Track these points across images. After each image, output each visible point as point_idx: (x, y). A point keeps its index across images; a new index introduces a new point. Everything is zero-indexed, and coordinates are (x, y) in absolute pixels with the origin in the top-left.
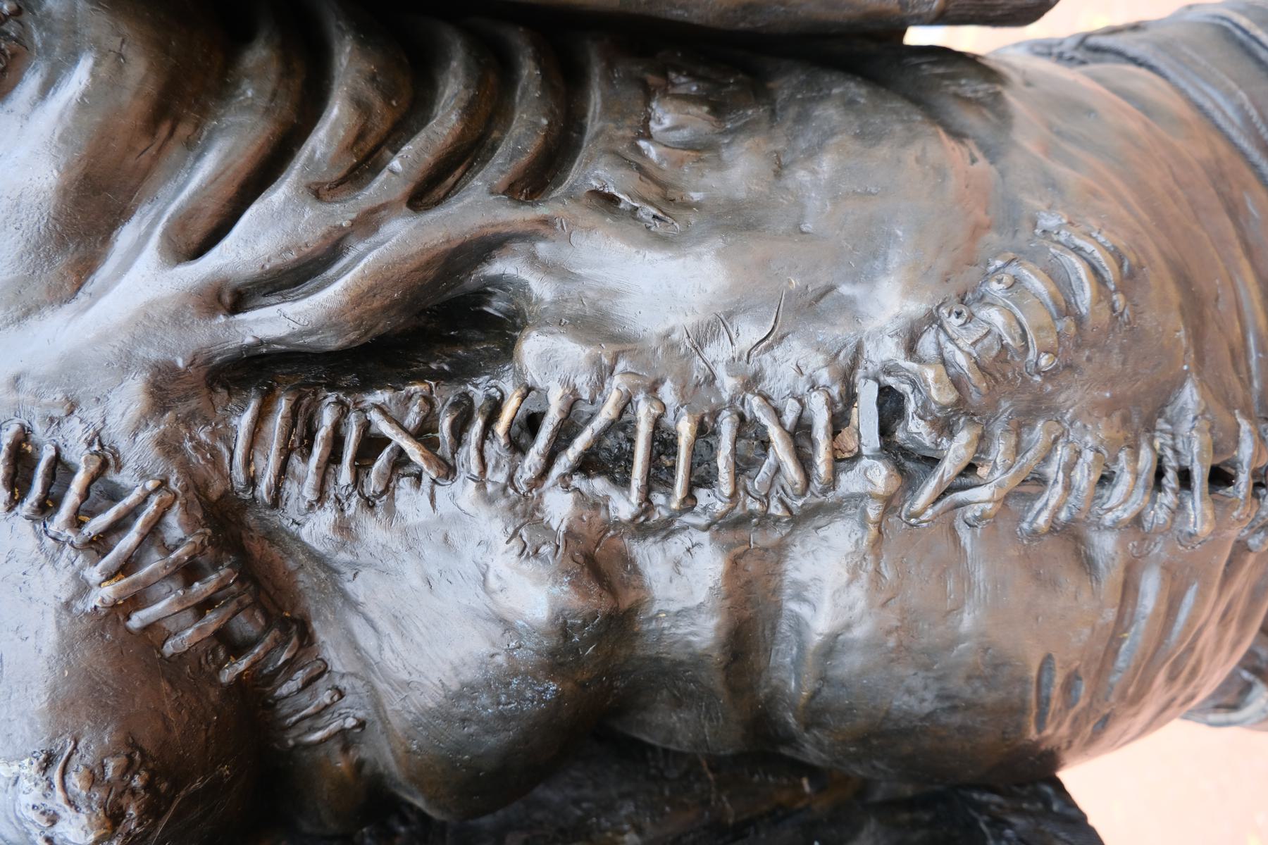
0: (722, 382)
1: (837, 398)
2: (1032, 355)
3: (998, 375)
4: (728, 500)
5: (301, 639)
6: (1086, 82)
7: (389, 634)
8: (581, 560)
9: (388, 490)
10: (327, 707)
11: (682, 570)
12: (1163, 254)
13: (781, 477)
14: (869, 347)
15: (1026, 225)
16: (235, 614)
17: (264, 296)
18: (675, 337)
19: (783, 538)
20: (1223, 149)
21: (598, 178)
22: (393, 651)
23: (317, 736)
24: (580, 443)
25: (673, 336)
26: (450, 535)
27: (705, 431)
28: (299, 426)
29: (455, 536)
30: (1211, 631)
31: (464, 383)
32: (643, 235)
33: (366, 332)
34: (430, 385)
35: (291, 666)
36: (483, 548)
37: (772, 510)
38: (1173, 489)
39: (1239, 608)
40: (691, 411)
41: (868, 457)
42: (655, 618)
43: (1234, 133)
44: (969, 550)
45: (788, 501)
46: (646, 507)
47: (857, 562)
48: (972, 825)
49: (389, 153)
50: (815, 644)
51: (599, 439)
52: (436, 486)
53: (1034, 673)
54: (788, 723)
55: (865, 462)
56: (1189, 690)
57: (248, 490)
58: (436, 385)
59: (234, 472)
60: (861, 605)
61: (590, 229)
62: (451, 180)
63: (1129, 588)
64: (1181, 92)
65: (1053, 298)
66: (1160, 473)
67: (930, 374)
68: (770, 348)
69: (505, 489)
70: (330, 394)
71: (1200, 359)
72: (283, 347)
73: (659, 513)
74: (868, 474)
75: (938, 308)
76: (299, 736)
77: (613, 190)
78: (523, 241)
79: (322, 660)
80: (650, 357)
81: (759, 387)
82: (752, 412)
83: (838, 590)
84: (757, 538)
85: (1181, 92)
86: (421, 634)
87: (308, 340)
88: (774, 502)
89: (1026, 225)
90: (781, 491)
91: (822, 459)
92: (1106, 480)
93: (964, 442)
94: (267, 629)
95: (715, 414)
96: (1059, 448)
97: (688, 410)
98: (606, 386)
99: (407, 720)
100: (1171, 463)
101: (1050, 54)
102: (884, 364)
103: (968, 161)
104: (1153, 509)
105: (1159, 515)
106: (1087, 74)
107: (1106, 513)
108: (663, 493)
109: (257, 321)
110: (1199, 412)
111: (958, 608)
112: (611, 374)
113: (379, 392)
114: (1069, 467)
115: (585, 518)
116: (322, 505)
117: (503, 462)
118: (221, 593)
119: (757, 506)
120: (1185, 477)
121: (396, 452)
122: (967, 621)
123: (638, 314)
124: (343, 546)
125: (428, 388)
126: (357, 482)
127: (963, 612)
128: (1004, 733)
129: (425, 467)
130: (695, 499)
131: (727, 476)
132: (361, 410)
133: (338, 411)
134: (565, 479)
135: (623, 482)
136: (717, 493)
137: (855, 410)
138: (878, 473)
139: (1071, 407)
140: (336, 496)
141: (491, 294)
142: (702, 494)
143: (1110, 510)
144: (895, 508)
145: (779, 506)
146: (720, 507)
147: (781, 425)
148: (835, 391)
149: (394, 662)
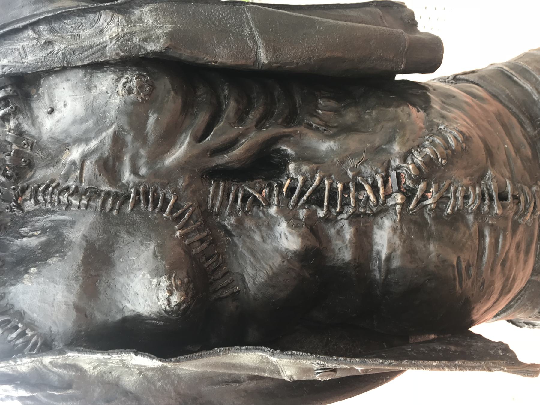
2: (440, 160)
9: (250, 210)
12: (480, 137)
14: (392, 162)
21: (306, 120)
27: (346, 189)
37: (367, 212)
39: (523, 246)
41: (395, 192)
43: (506, 103)
45: (372, 208)
53: (455, 263)
55: (394, 195)
63: (482, 236)
65: (444, 145)
67: (411, 167)
75: (411, 149)
82: (359, 181)
101: (445, 82)
102: (397, 166)
114: (455, 191)
126: (243, 207)
135: (321, 206)
146: (351, 211)
147: (368, 184)
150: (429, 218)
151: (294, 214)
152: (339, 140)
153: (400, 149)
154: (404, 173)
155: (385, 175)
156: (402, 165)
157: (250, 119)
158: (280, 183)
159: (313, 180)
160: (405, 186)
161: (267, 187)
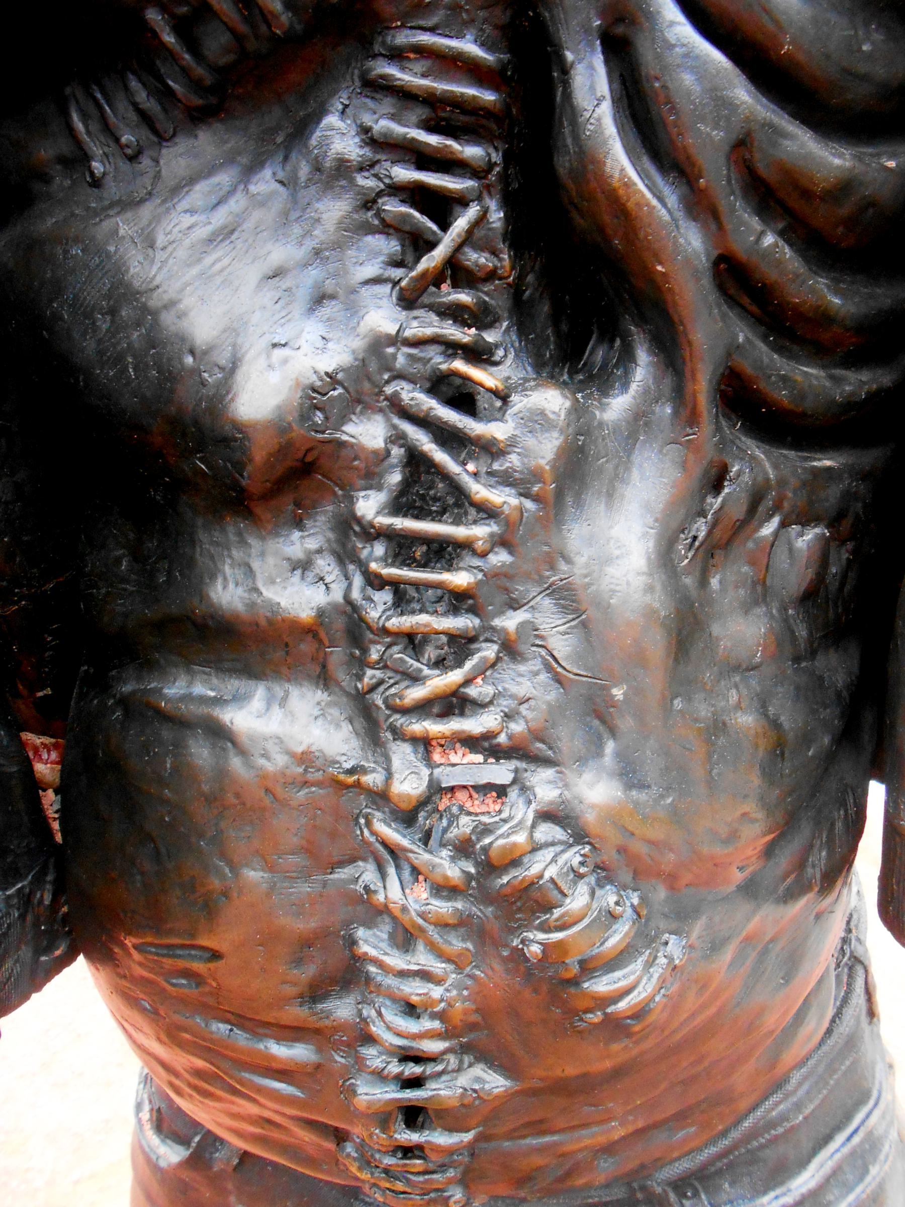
0: (511, 618)
1: (495, 741)
2: (541, 936)
3: (519, 904)
4: (381, 624)
5: (198, 109)
6: (818, 972)
7: (210, 223)
8: (309, 459)
9: (387, 227)
10: (117, 140)
11: (298, 572)
13: (406, 683)
14: (548, 773)
15: (674, 926)
16: (232, 31)
17: (621, 75)
18: (563, 566)
19: (338, 684)
20: (744, 1105)
21: (739, 474)
22: (189, 228)
23: (79, 126)
24: (440, 456)
25: (563, 563)
26: (333, 303)
28: (462, 118)
29: (330, 309)
30: (253, 1110)
31: (510, 318)
32: (674, 525)
33: (572, 203)
34: (509, 277)
35: (165, 95)
36: (320, 343)
37: (369, 672)
38: (402, 1073)
39: (276, 1135)
40: (479, 583)
41: (431, 774)
42: (243, 543)
43: (759, 1113)
44: (335, 876)
46: (370, 533)
47: (314, 762)
48: (18, 875)
49: (780, 226)
50: (221, 716)
51: (446, 477)
52: (390, 286)
54: (125, 683)
55: (425, 772)
56: (187, 1090)
57: (385, 49)
58: (508, 284)
59: (408, 32)
60: (269, 767)
61: (684, 465)
62: (746, 301)
64: (803, 1062)
66: (418, 1059)
68: (548, 668)
69: (389, 369)
70: (500, 154)
71: (533, 1092)
72: (558, 99)
73: (364, 548)
74: (413, 775)
76: (77, 102)
77: (726, 490)
78: (673, 390)
79: (174, 135)
80: (540, 538)
81: (506, 658)
82: (479, 650)
83: (282, 742)
84: (337, 654)
85: (803, 1062)
86: (213, 264)
87: (567, 131)
88: (378, 674)
89: (674, 926)
90: (392, 681)
91: (428, 727)
92: (411, 1009)
93: (449, 873)
94: (214, 69)
95: (474, 610)
96: (443, 965)
97: (481, 581)
98: (507, 489)
99: (107, 243)
100: (430, 1069)
102: (531, 789)
103: (740, 865)
104: (381, 1053)
105: (373, 1057)
106: (827, 969)
107: (376, 1010)
108: (386, 553)
109: (591, 67)
110: (481, 1094)
111: (270, 867)
112: (521, 495)
113: (502, 215)
115: (356, 463)
116: (367, 144)
117: (419, 366)
118: (257, 11)
119: (374, 656)
120: (416, 1082)
121: (431, 238)
122: (254, 875)
123: (588, 522)
124: (318, 168)
125: (506, 274)
126: (397, 190)
127: (263, 870)
128: (133, 912)
129: (414, 274)
130: (381, 588)
131: (408, 624)
132: (481, 193)
133: (480, 167)
134: (398, 438)
135: (398, 506)
136: (388, 613)
137: (479, 758)
138: (415, 786)
139: (486, 975)
140: (378, 161)
141: (612, 341)
142: (384, 597)
143: (380, 1014)
144: (374, 803)
145: (374, 681)
146: (373, 614)
147: (468, 682)
148: (502, 739)
149: (177, 229)
150: (343, 876)
151: (366, 398)
152: (650, 589)
153: (593, 806)
154: (500, 811)
155: (499, 745)
156: (533, 806)
157: (762, 234)
158: (492, 354)
159: (493, 480)
160: (455, 810)
161: (479, 298)
